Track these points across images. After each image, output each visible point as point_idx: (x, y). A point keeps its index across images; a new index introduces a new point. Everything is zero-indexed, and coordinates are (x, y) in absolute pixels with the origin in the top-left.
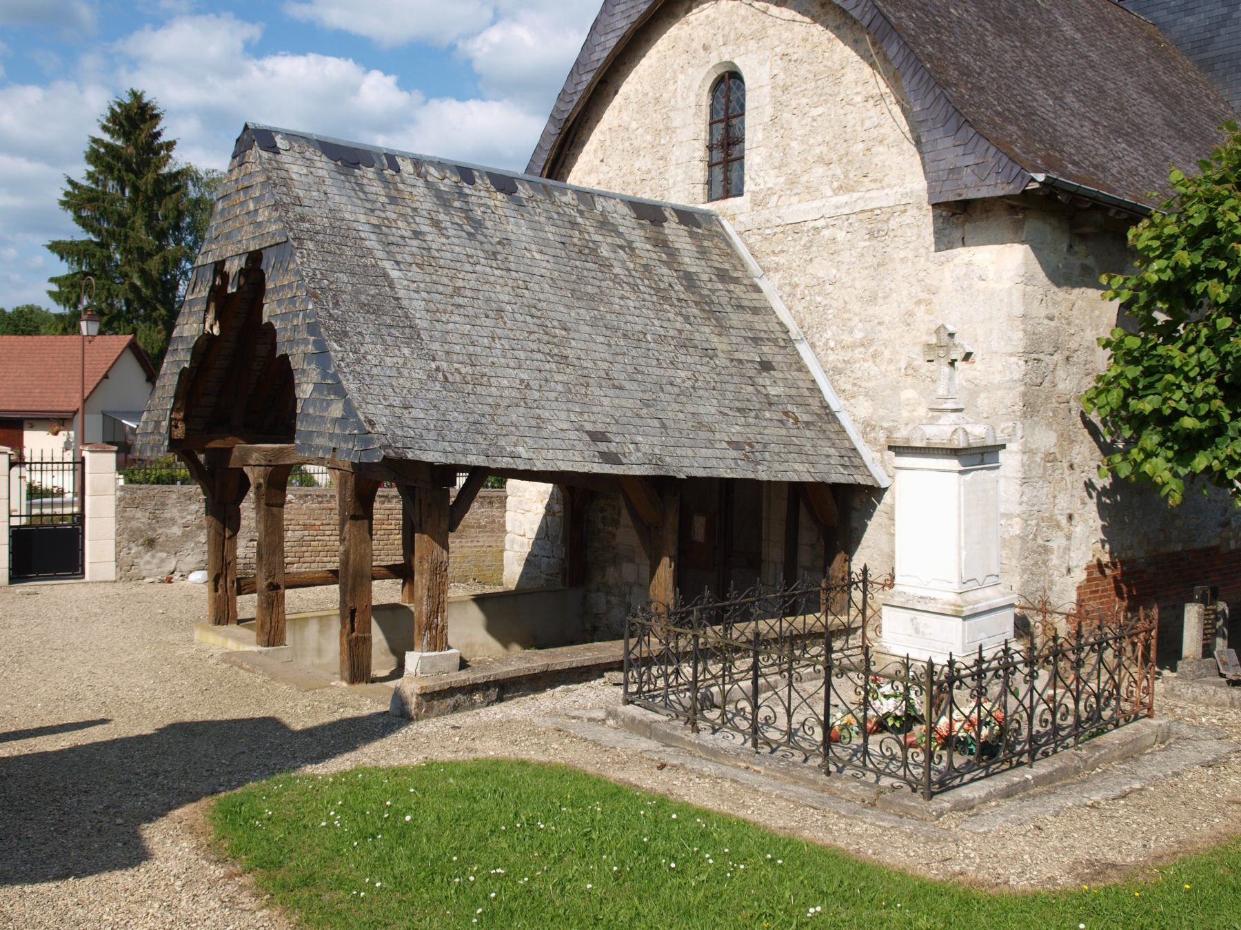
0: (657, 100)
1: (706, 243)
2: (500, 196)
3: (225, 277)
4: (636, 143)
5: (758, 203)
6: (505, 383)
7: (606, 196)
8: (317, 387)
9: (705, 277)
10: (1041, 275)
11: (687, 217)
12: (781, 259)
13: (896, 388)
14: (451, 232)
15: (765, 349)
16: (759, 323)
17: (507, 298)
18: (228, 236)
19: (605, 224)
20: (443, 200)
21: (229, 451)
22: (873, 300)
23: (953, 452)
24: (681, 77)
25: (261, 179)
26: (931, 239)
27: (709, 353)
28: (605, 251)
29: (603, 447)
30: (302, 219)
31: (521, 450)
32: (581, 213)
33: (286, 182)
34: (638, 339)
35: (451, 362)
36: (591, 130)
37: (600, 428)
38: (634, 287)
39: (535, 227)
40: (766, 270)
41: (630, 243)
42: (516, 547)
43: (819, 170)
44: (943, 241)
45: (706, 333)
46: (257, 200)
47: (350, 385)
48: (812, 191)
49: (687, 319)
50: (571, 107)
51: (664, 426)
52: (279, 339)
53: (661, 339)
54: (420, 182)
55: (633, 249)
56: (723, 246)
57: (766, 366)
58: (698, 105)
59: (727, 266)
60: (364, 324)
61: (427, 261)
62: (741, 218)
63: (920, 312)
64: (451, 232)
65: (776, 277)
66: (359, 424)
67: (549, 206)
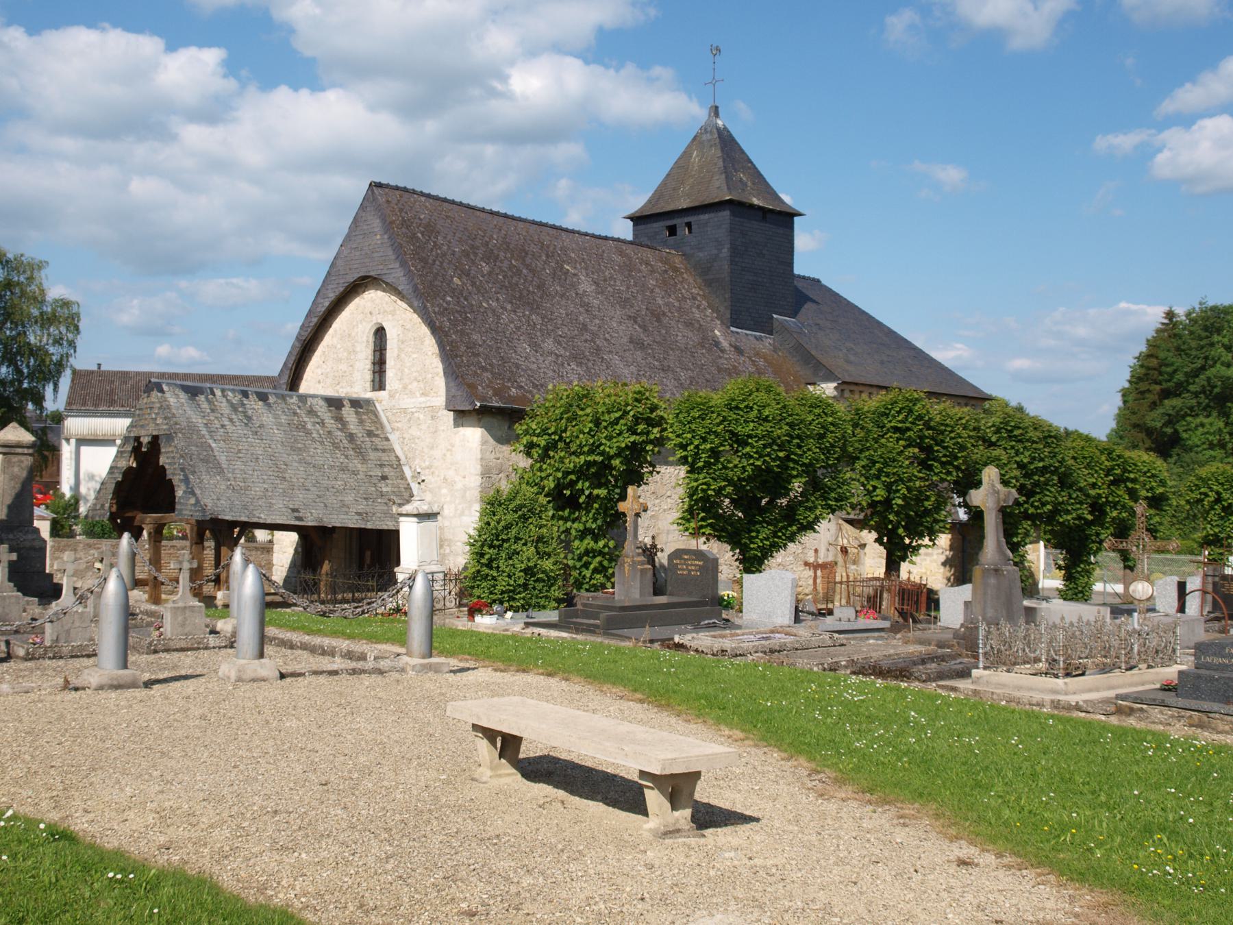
0: (349, 335)
1: (364, 417)
2: (260, 403)
3: (140, 444)
4: (340, 356)
5: (391, 396)
6: (258, 489)
7: (313, 396)
8: (185, 492)
9: (360, 435)
10: (491, 440)
11: (356, 403)
12: (399, 425)
13: (439, 488)
14: (237, 424)
15: (385, 470)
16: (384, 457)
17: (260, 452)
18: (142, 426)
19: (311, 412)
20: (234, 408)
21: (134, 518)
22: (432, 448)
23: (415, 516)
24: (360, 326)
25: (158, 405)
26: (452, 422)
27: (355, 473)
28: (309, 426)
29: (296, 514)
30: (176, 424)
31: (262, 516)
32: (299, 407)
33: (169, 407)
34: (319, 468)
35: (235, 481)
36: (318, 344)
37: (296, 507)
38: (322, 443)
39: (276, 417)
40: (393, 429)
41: (323, 420)
42: (279, 573)
43: (415, 384)
44: (457, 425)
45: (356, 464)
46: (156, 414)
47: (198, 492)
48: (412, 393)
49: (346, 457)
50: (306, 334)
51: (326, 506)
52: (168, 472)
53: (332, 467)
54: (224, 400)
55: (323, 424)
56: (373, 417)
57: (384, 478)
58: (368, 342)
59: (373, 428)
60: (202, 467)
61: (227, 438)
62: (384, 403)
63: (448, 454)
64: (237, 424)
65: (397, 433)
66: (201, 506)
67: (283, 405)
